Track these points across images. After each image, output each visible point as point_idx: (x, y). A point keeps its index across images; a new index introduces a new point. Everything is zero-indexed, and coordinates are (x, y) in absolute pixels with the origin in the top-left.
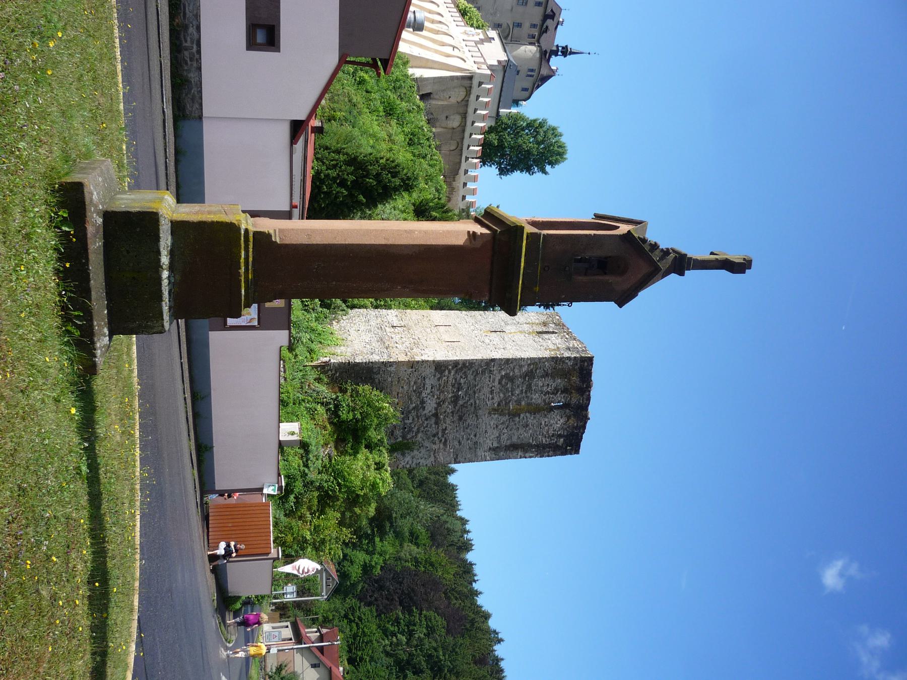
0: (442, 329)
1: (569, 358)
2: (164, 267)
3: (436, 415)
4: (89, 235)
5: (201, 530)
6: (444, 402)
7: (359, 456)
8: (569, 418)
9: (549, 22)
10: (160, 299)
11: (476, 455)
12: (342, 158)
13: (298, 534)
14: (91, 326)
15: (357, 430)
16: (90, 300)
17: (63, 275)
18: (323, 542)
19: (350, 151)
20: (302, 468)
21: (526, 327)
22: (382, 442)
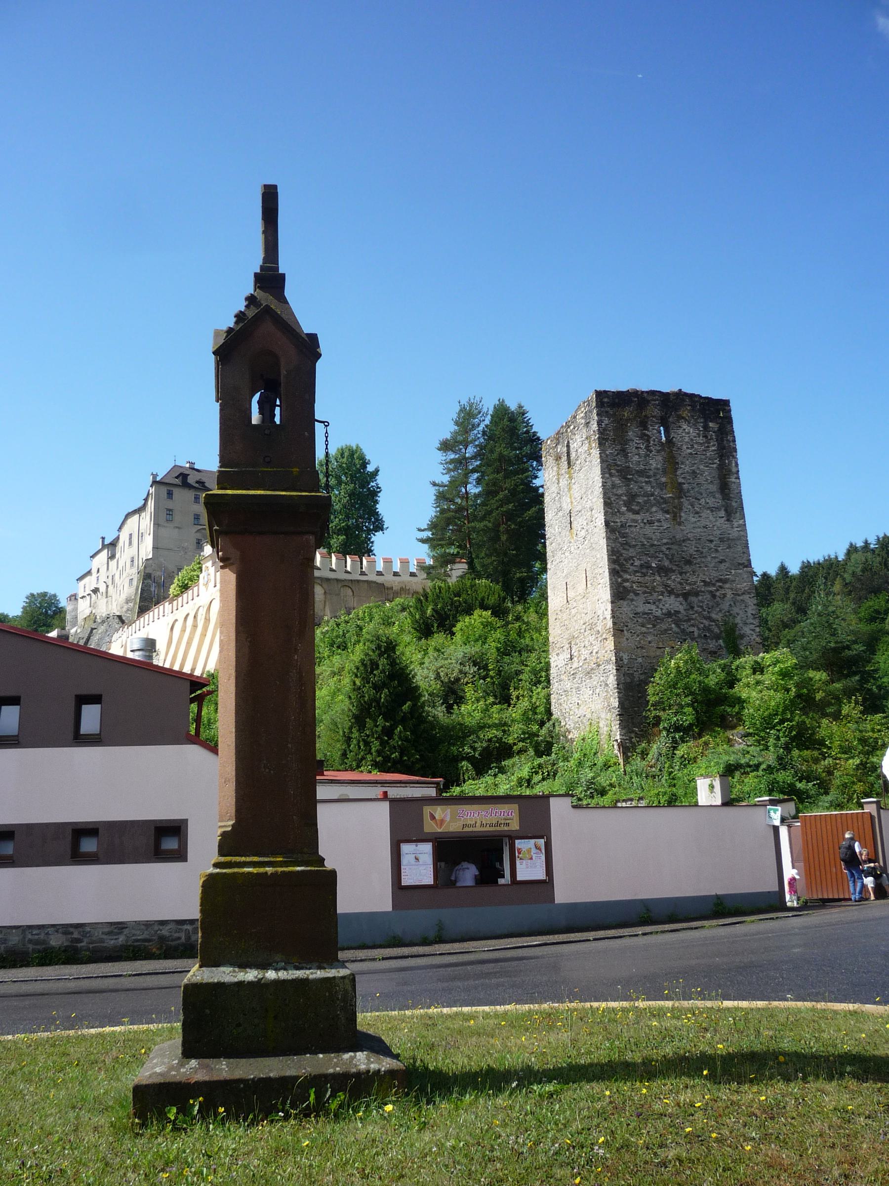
0: (571, 594)
2: (260, 976)
3: (686, 596)
4: (207, 1078)
5: (842, 909)
6: (666, 586)
7: (744, 695)
8: (680, 417)
9: (191, 480)
10: (305, 982)
11: (739, 539)
12: (355, 734)
13: (852, 776)
14: (335, 1076)
15: (709, 700)
16: (298, 1077)
17: (267, 1112)
18: (863, 741)
19: (347, 724)
20: (760, 773)
21: (563, 482)
22: (725, 665)
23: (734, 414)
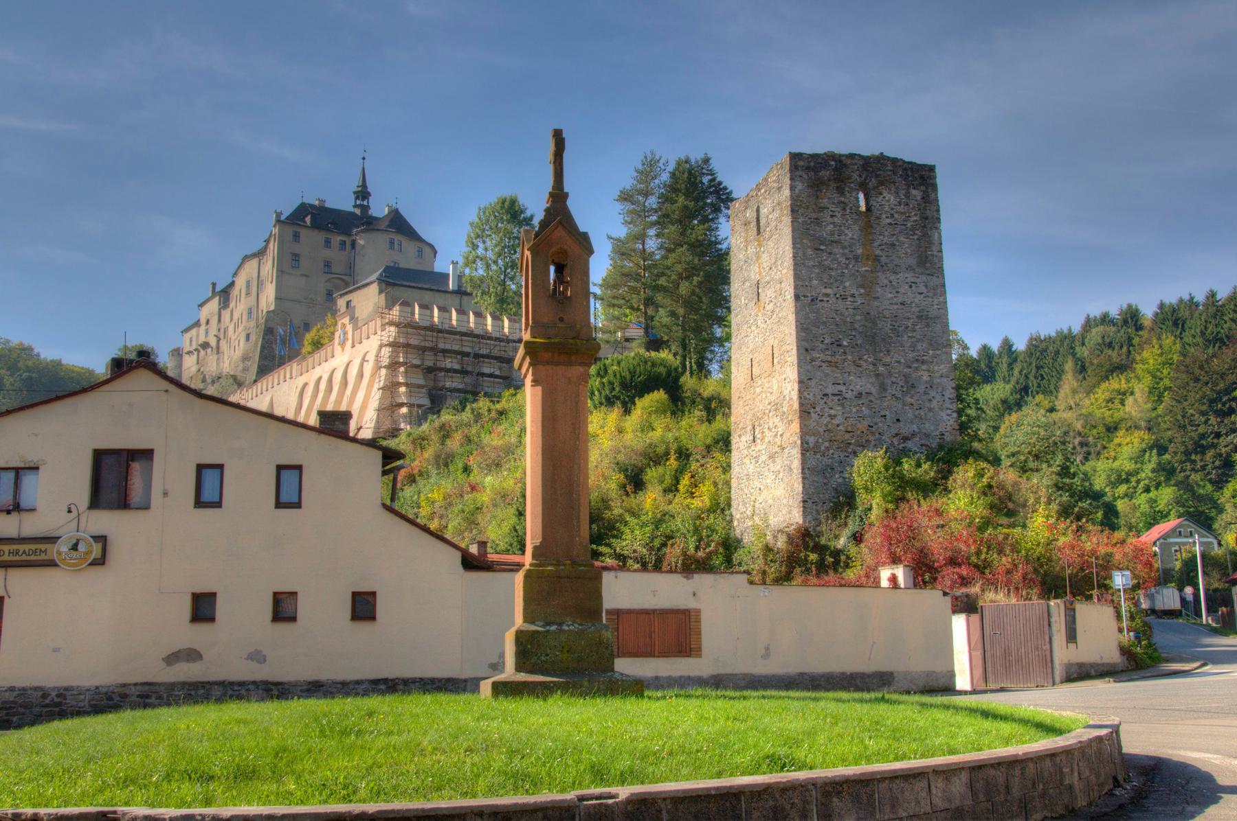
1: (792, 188)
11: (938, 317)
23: (939, 181)
